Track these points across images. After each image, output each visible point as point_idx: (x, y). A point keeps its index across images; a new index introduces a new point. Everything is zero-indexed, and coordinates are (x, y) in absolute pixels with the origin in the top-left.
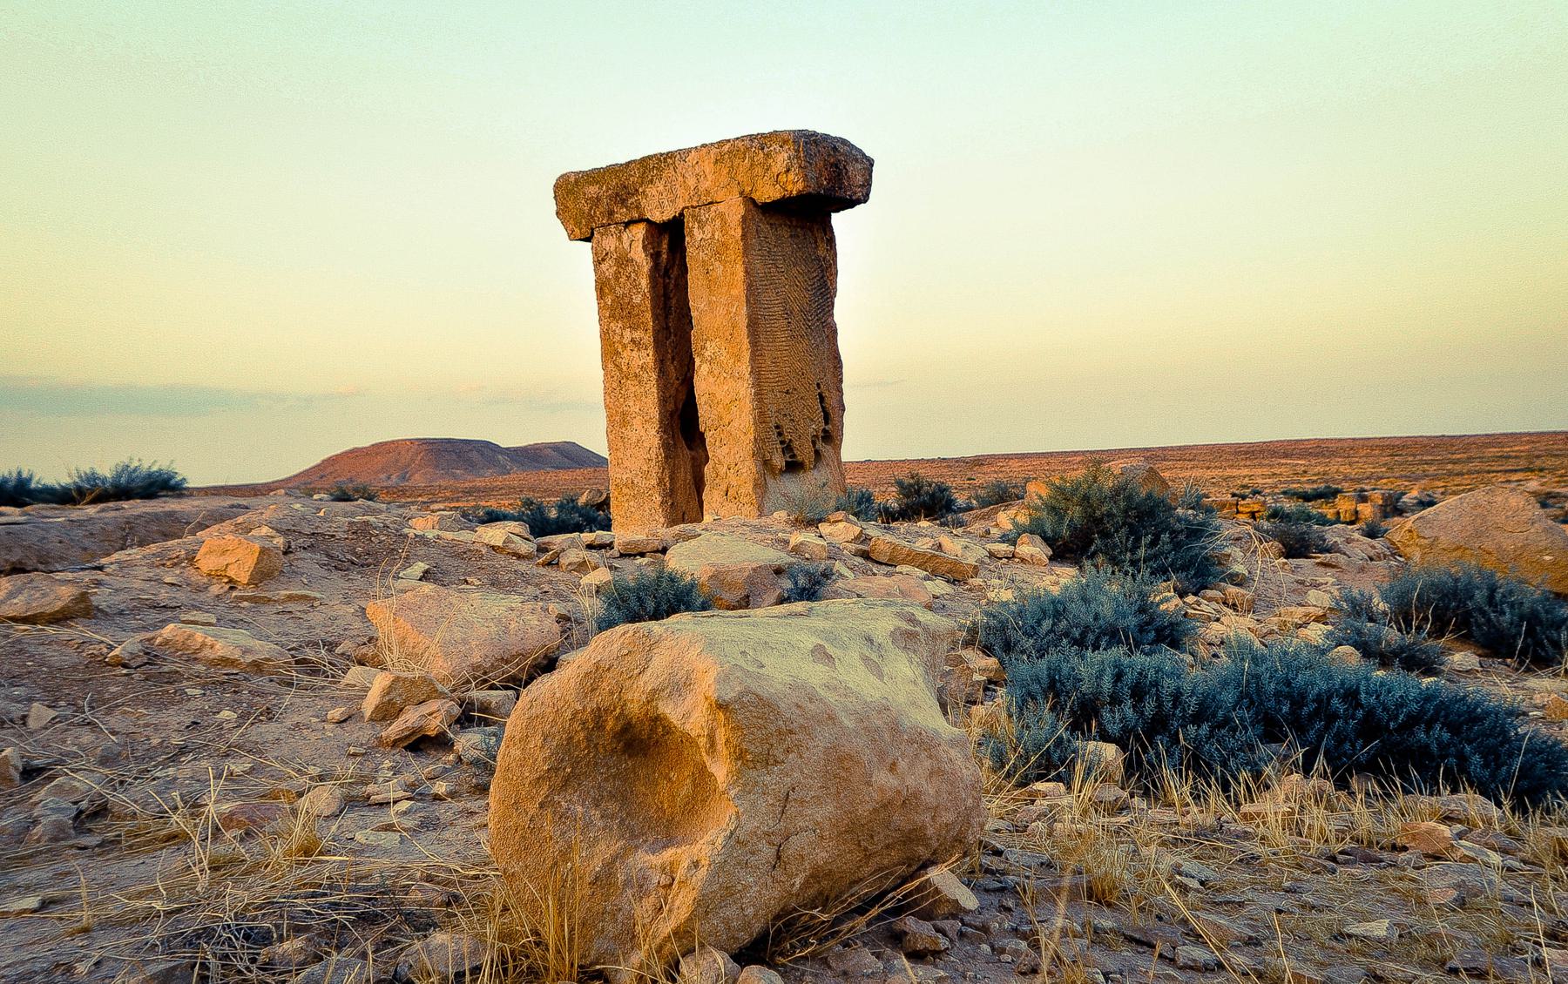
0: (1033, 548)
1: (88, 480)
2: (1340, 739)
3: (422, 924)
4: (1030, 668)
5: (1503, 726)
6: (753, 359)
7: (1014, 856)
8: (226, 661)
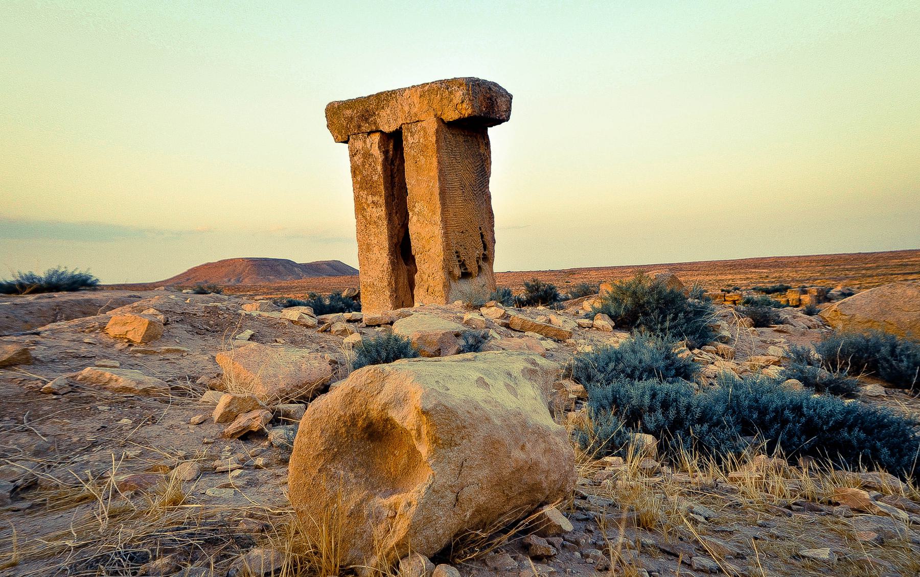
0: (603, 322)
1: (28, 279)
2: (791, 435)
3: (246, 544)
4: (602, 390)
5: (904, 431)
6: (442, 213)
7: (594, 499)
8: (125, 389)
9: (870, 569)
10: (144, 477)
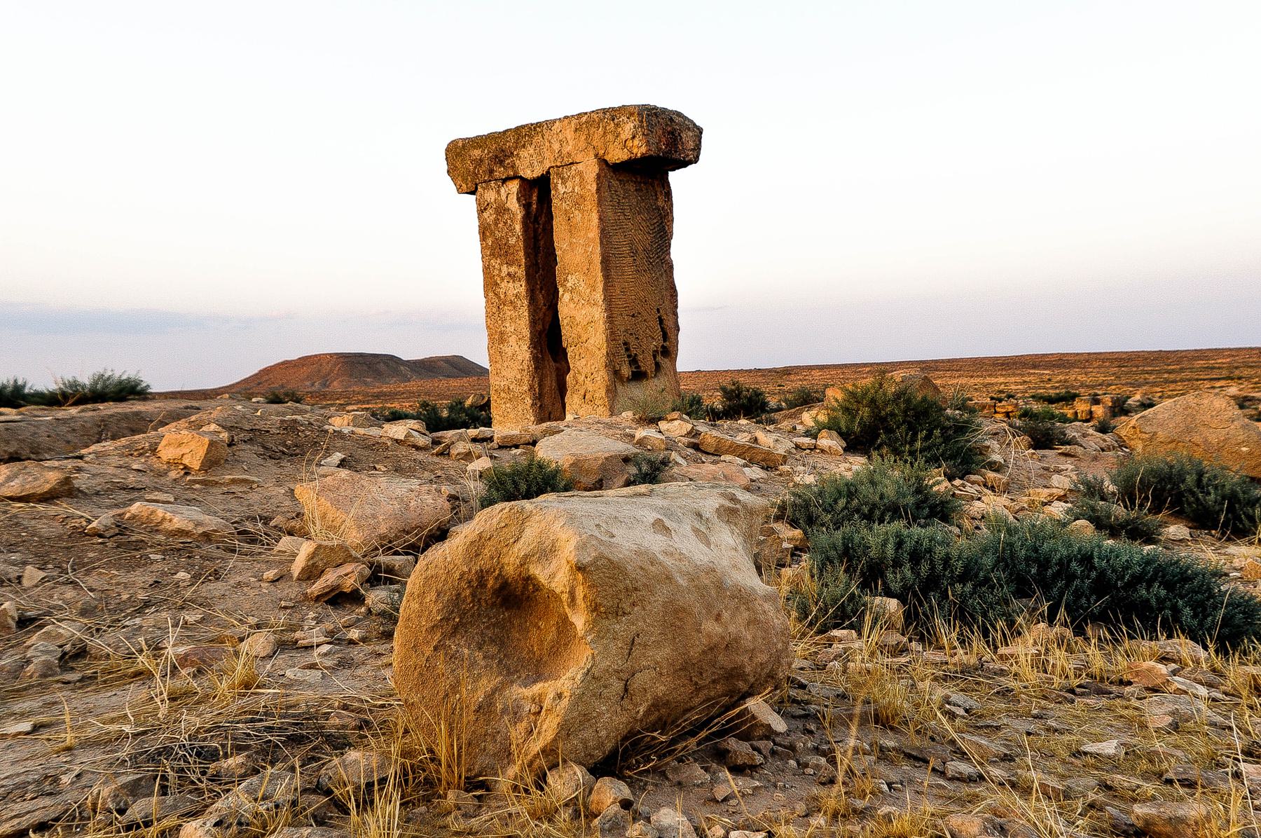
0: (828, 441)
2: (1078, 594)
3: (340, 744)
5: (1209, 584)
6: (605, 289)
7: (816, 689)
9: (1161, 761)
10: (207, 650)
